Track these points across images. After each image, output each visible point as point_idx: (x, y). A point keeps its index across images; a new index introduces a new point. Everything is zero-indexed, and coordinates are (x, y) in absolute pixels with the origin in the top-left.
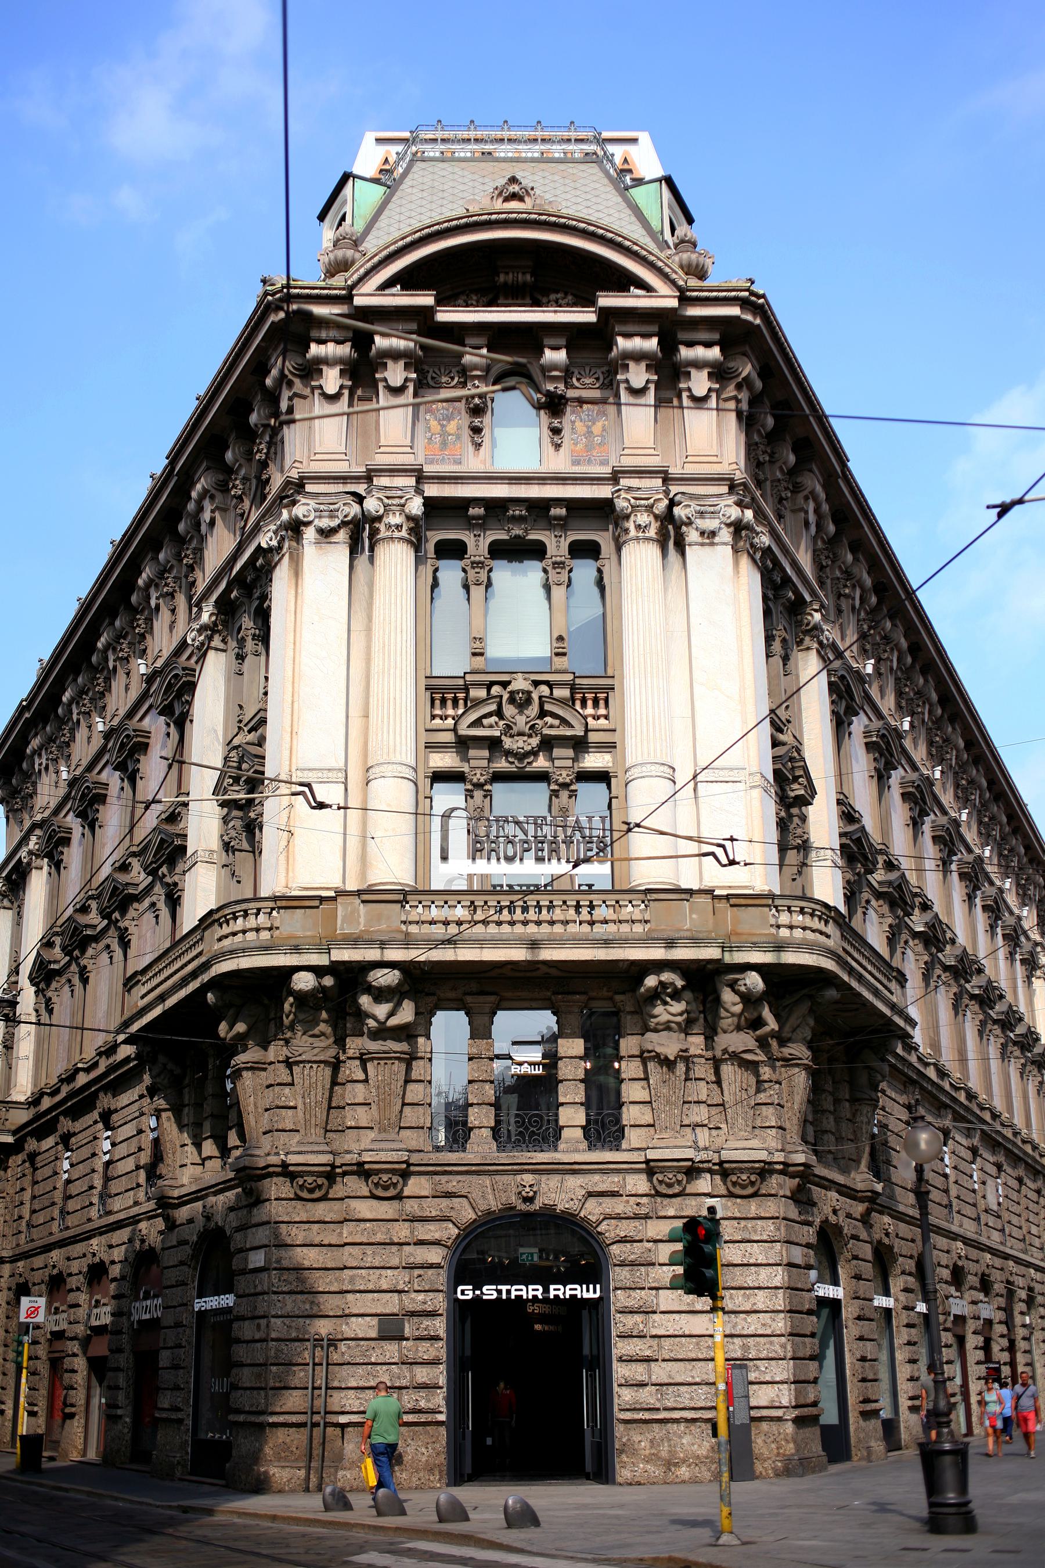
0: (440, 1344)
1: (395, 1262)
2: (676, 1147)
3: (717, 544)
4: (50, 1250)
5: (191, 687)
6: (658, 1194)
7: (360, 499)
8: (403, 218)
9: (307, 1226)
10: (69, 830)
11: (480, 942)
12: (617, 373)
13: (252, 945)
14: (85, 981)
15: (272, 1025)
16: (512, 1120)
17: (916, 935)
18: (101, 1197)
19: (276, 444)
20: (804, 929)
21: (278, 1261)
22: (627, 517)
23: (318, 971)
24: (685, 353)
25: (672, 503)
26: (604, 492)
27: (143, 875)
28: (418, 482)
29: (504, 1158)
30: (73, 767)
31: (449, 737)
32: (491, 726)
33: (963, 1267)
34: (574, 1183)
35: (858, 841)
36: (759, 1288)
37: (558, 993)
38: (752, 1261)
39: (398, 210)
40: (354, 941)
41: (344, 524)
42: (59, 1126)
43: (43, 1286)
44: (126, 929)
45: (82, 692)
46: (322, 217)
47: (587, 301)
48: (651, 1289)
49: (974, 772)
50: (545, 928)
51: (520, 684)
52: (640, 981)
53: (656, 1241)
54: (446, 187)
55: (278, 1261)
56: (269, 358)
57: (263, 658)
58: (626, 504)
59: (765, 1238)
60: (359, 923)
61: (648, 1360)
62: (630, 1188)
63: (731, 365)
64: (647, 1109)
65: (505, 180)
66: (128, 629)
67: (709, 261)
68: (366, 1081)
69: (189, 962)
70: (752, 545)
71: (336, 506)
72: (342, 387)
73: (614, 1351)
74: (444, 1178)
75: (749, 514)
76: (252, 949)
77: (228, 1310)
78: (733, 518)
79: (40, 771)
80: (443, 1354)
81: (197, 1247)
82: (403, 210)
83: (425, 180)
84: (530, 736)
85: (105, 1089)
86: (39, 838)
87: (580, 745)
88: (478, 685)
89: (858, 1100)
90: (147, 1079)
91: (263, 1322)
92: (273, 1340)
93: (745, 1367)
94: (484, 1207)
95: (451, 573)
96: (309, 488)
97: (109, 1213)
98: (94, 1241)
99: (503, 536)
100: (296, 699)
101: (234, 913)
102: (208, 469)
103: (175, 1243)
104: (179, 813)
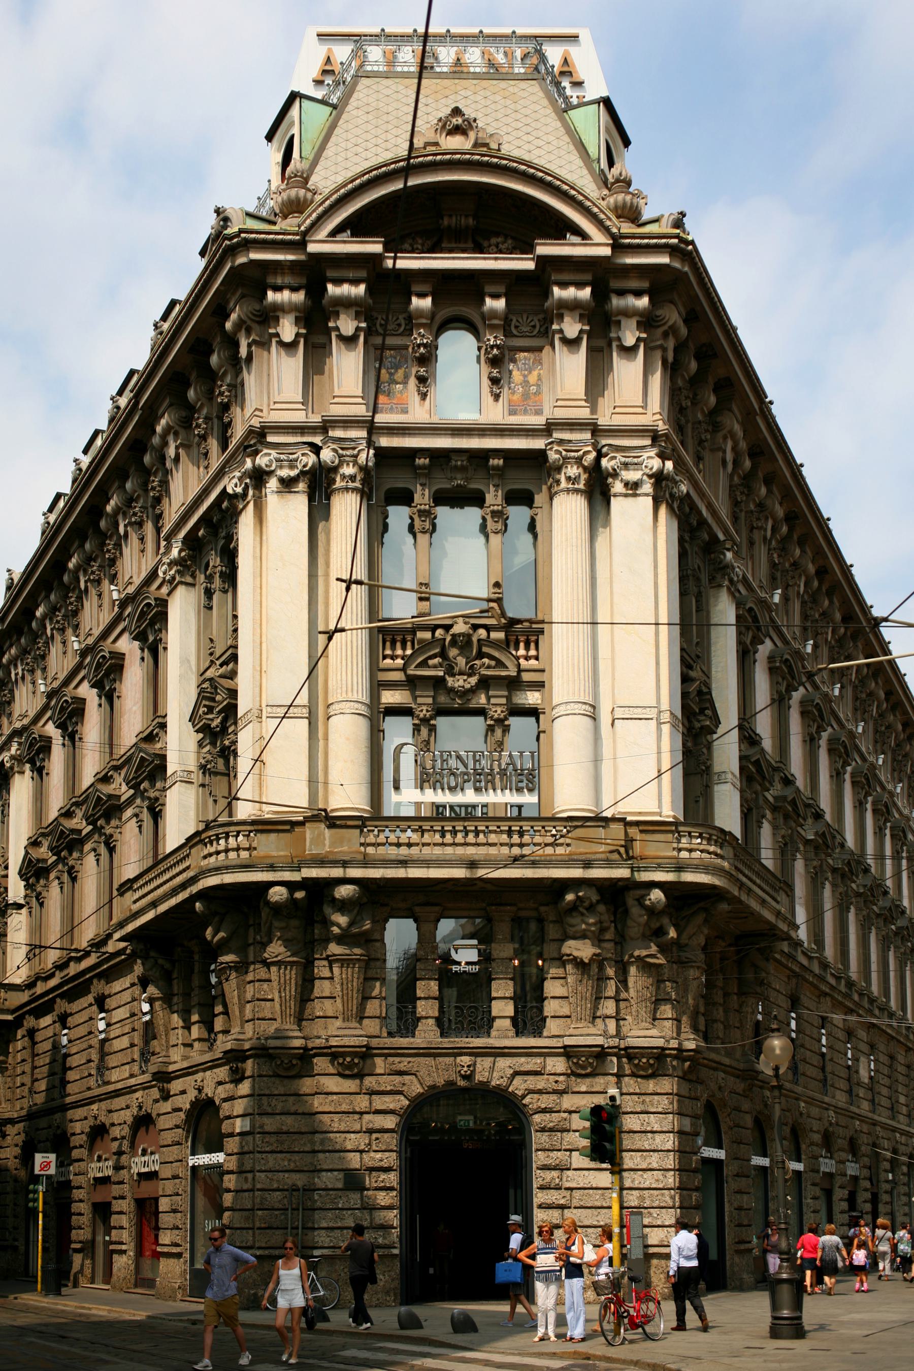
0: (395, 1193)
1: (357, 1127)
2: (588, 1035)
3: (639, 495)
4: (54, 1113)
5: (162, 617)
6: (573, 1074)
7: (316, 449)
8: (350, 145)
9: (284, 1098)
10: (49, 740)
11: (427, 863)
12: (552, 323)
13: (234, 863)
14: (74, 879)
15: (251, 930)
16: (453, 1013)
17: (807, 842)
18: (98, 1069)
19: (237, 389)
20: (702, 851)
21: (262, 1127)
22: (559, 469)
23: (291, 886)
24: (616, 302)
25: (600, 455)
26: (538, 444)
27: (124, 787)
28: (370, 433)
29: (446, 1042)
30: (49, 680)
31: (398, 676)
32: (435, 667)
33: (833, 1133)
34: (504, 1064)
35: (757, 763)
36: (654, 1151)
37: (492, 905)
38: (649, 1129)
39: (344, 136)
40: (321, 862)
41: (302, 473)
42: (56, 1007)
43: (48, 1144)
44: (111, 836)
45: (53, 610)
46: (270, 137)
47: (527, 248)
48: (566, 1150)
49: (873, 684)
50: (482, 850)
51: (460, 628)
52: (561, 894)
53: (570, 1112)
54: (390, 109)
55: (262, 1127)
56: (228, 302)
57: (230, 594)
58: (557, 456)
59: (660, 1110)
60: (324, 845)
61: (562, 1207)
62: (549, 1068)
63: (659, 313)
64: (564, 1003)
65: (449, 111)
66: (97, 552)
67: (642, 202)
68: (332, 978)
69: (178, 874)
70: (672, 495)
71: (295, 456)
72: (298, 335)
73: (535, 1200)
74: (397, 1059)
75: (669, 465)
76: (234, 867)
77: (219, 1166)
78: (654, 470)
79: (16, 680)
80: (396, 1201)
81: (189, 1113)
82: (350, 136)
83: (371, 100)
84: (470, 675)
85: (99, 976)
86: (20, 744)
87: (514, 684)
88: (424, 628)
89: (744, 994)
90: (138, 969)
91: (250, 1176)
92: (258, 1190)
93: (641, 1213)
94: (429, 1082)
95: (398, 516)
96: (271, 439)
97: (108, 1083)
98: (95, 1107)
99: (446, 485)
100: (264, 639)
101: (217, 835)
102: (171, 405)
103: (169, 1110)
104: (157, 734)
